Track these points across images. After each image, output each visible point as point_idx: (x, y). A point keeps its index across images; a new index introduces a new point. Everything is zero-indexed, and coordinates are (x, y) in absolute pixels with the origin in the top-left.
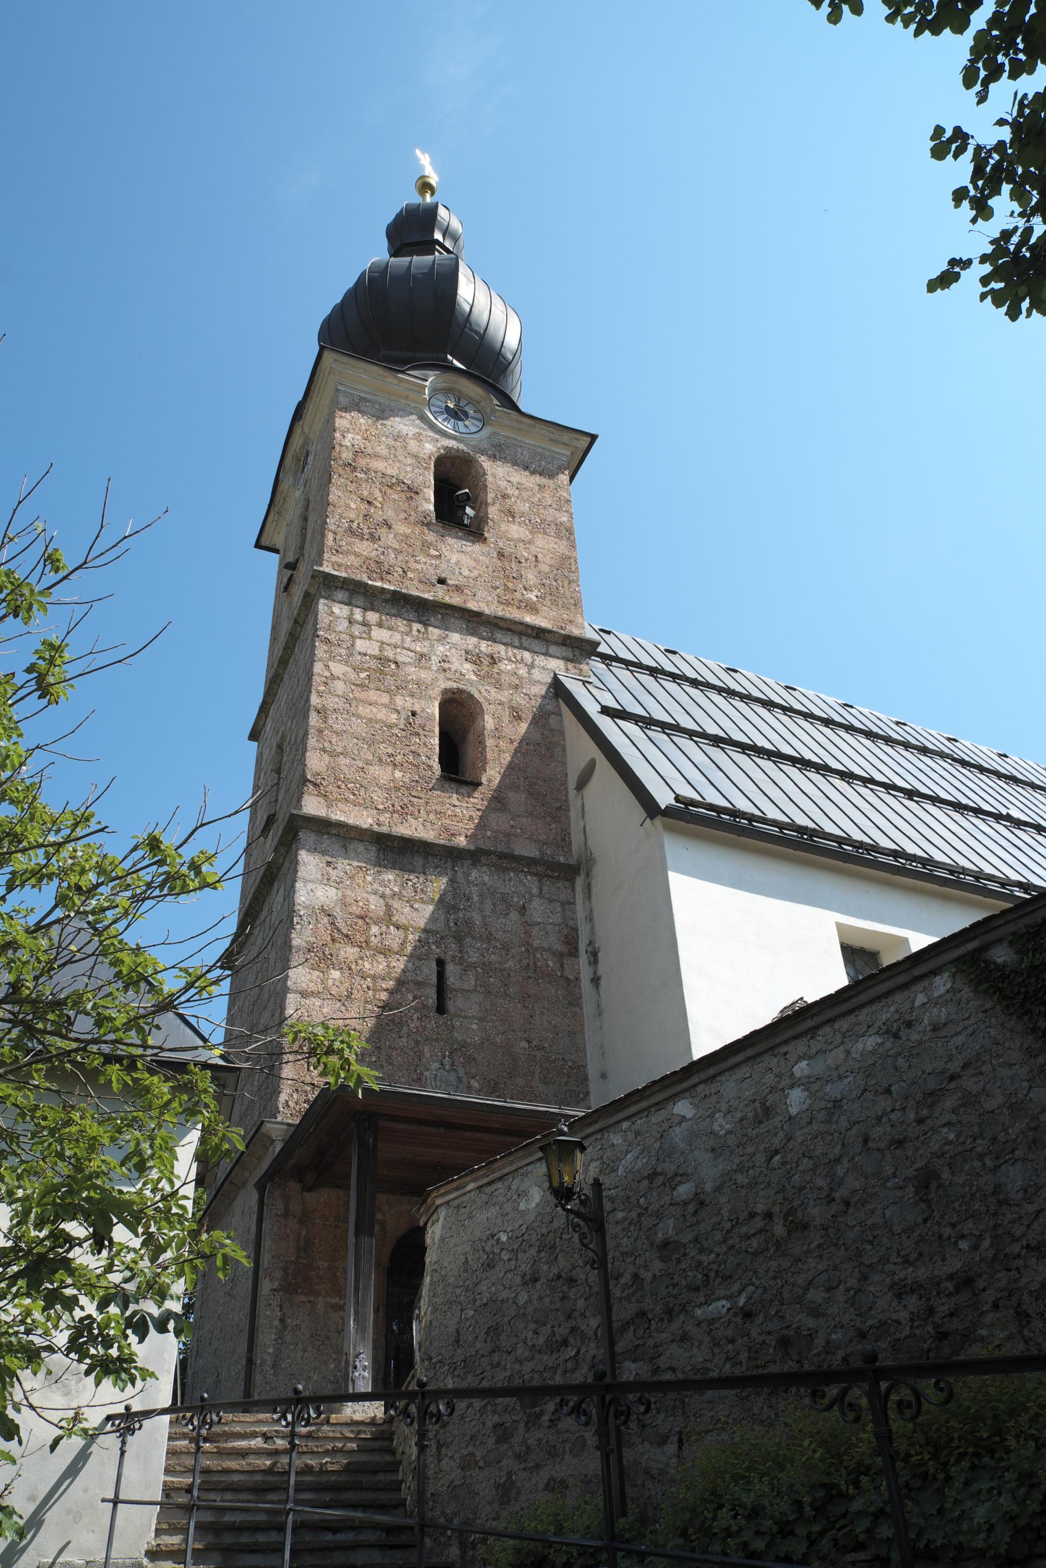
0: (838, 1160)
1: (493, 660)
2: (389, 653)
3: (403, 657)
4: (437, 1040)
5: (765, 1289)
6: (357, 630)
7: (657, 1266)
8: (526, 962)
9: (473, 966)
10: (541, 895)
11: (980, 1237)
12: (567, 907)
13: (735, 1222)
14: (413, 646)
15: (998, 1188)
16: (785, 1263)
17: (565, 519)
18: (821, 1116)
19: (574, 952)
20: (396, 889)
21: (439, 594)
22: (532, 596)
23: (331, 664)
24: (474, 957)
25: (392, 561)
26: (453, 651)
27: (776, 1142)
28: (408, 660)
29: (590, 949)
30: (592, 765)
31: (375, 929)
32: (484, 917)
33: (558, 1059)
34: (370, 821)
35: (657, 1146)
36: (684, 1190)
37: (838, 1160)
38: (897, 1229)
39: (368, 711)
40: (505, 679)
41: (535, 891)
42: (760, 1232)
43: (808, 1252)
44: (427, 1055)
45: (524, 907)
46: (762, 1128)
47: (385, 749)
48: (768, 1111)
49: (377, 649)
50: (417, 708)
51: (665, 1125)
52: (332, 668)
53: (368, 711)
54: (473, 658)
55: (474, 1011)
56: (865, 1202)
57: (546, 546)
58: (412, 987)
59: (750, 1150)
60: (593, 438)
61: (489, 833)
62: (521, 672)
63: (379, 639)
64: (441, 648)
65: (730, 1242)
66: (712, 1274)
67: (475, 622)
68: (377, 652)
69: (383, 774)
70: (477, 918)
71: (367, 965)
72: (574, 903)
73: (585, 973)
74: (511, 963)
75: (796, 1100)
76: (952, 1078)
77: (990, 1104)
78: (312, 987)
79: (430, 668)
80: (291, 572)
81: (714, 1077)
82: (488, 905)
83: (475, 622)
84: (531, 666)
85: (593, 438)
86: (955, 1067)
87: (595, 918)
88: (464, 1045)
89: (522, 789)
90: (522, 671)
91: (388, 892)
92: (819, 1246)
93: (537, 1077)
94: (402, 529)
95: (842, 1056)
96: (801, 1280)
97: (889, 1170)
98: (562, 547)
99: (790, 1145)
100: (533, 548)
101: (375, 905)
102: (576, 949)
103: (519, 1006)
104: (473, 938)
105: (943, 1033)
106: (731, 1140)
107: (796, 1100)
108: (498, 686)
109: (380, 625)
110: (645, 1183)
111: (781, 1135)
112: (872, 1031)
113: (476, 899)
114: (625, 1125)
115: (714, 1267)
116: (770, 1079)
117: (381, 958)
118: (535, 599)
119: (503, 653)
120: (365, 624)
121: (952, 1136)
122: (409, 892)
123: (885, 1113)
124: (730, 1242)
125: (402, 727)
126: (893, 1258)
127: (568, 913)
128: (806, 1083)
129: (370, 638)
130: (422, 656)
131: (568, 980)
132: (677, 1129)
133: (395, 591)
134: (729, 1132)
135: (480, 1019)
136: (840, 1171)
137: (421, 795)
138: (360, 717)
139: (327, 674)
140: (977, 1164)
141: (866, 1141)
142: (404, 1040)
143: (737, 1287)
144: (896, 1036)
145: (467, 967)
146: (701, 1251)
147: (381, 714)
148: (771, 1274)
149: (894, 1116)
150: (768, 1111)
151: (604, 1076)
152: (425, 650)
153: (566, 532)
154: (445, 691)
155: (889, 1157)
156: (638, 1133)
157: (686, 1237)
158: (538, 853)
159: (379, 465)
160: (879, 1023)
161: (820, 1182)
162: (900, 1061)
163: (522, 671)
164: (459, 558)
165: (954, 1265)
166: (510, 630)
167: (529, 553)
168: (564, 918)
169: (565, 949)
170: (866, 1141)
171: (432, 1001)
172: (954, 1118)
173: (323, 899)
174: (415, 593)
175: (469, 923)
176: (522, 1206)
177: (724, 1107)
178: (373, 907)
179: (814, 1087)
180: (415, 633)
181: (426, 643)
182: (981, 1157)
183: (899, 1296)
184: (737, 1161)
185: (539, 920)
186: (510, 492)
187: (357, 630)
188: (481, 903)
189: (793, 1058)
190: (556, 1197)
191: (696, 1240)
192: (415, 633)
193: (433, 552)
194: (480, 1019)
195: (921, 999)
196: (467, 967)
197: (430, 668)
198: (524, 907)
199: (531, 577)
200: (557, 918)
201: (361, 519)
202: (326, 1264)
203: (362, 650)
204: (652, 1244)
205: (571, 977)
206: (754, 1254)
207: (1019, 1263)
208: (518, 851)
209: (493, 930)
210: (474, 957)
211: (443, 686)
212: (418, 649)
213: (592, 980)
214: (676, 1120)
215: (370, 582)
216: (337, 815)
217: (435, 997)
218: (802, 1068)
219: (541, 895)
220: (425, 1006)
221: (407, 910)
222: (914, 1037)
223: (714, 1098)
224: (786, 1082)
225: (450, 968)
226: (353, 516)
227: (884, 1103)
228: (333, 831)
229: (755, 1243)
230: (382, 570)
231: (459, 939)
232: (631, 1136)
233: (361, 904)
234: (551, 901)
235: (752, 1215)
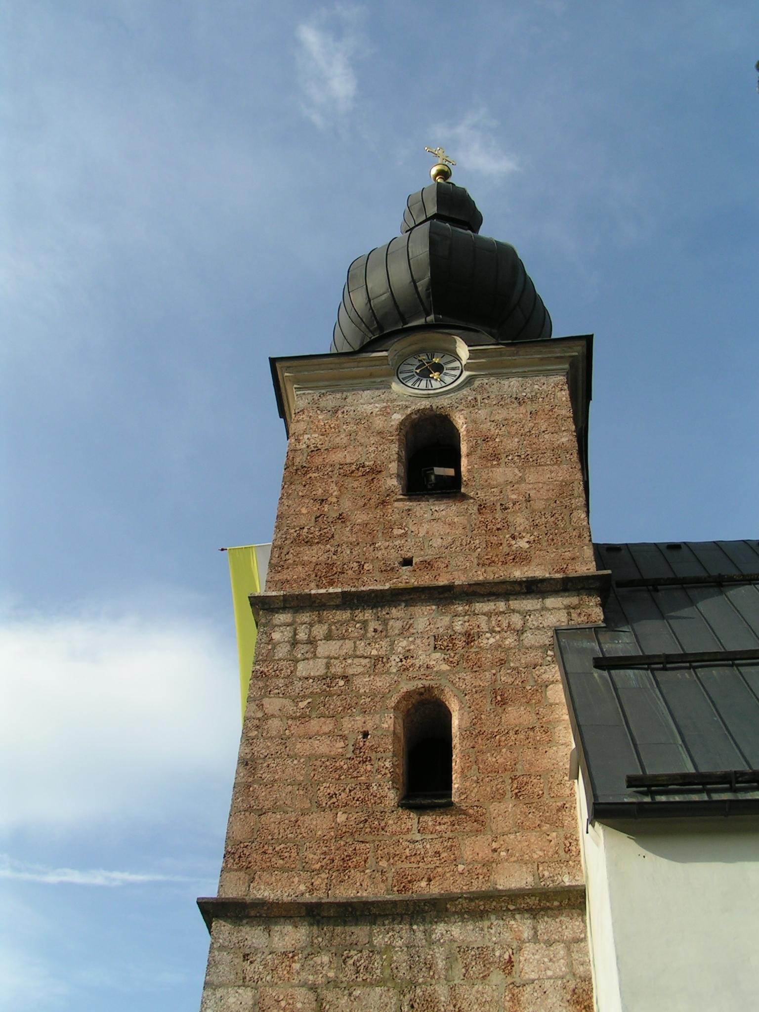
22: (523, 544)
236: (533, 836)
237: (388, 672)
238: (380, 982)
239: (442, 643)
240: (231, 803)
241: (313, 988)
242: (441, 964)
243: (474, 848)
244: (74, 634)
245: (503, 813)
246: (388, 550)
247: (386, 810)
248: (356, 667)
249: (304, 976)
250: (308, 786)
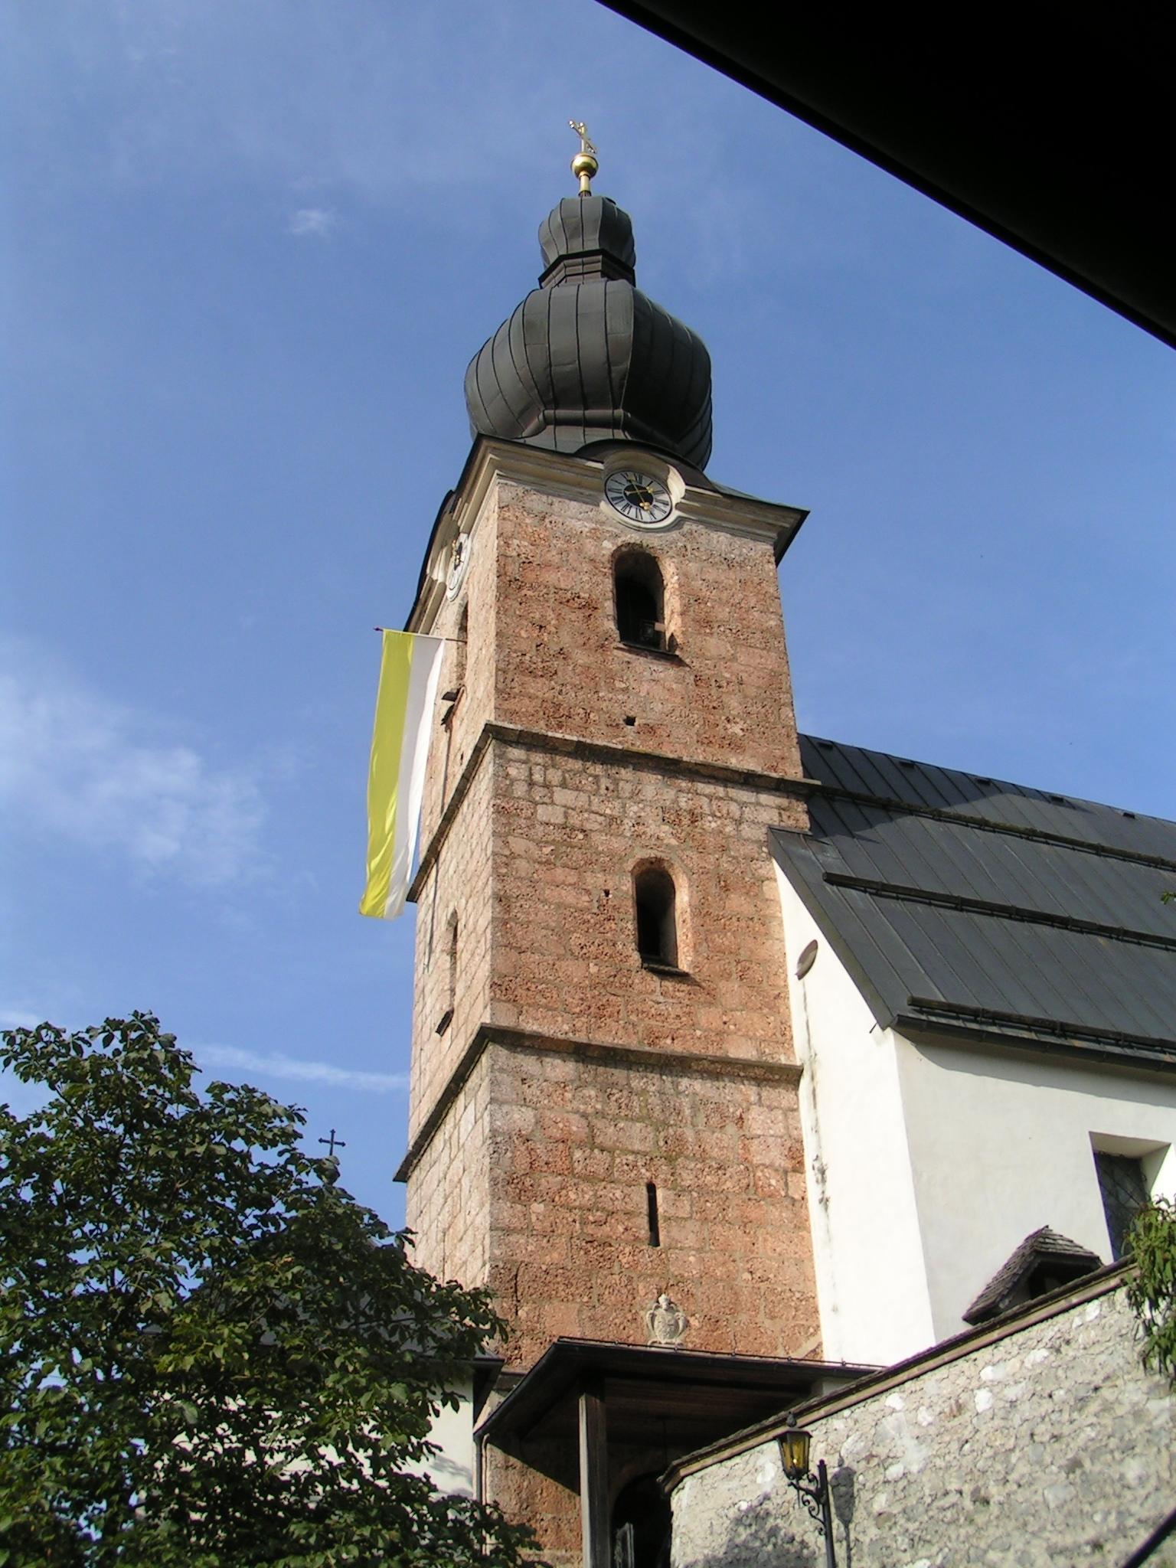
0: (1012, 1450)
1: (694, 817)
2: (575, 820)
3: (594, 823)
4: (651, 1276)
5: (956, 1552)
6: (538, 794)
7: (873, 1532)
8: (745, 1182)
9: (688, 1189)
10: (760, 1102)
11: (1109, 1513)
12: (790, 1114)
13: (935, 1498)
14: (602, 809)
15: (1122, 1477)
16: (971, 1530)
17: (772, 623)
18: (1001, 1413)
19: (798, 1167)
20: (599, 1106)
21: (630, 740)
22: (736, 729)
23: (510, 839)
24: (688, 1179)
25: (572, 702)
26: (648, 809)
27: (967, 1434)
28: (596, 827)
29: (817, 1164)
30: (813, 946)
31: (578, 1154)
32: (697, 1132)
33: (783, 1291)
34: (566, 1027)
35: (873, 1431)
36: (895, 1471)
37: (1012, 1450)
38: (1052, 1505)
39: (555, 894)
40: (711, 841)
41: (753, 1098)
42: (953, 1505)
43: (989, 1521)
44: (642, 1292)
45: (741, 1118)
46: (955, 1422)
47: (576, 939)
48: (960, 1408)
49: (561, 816)
50: (610, 886)
51: (879, 1415)
52: (512, 845)
53: (555, 894)
54: (671, 816)
55: (691, 1241)
56: (1031, 1484)
57: (752, 663)
58: (621, 1216)
59: (947, 1438)
60: (804, 514)
61: (698, 1033)
62: (728, 829)
63: (564, 802)
64: (635, 808)
65: (931, 1513)
66: (916, 1539)
67: (671, 768)
68: (561, 820)
69: (574, 970)
70: (689, 1135)
71: (572, 1196)
72: (796, 1110)
73: (813, 1193)
74: (729, 1184)
75: (983, 1400)
76: (1096, 1389)
77: (1120, 1411)
78: (516, 1223)
79: (622, 835)
80: (450, 703)
81: (918, 1376)
82: (701, 1119)
83: (671, 768)
84: (739, 822)
85: (804, 514)
86: (1097, 1380)
87: (822, 1129)
88: (680, 1280)
89: (734, 976)
90: (729, 829)
91: (590, 1110)
92: (997, 1518)
93: (762, 1313)
94: (581, 657)
95: (1018, 1365)
96: (983, 1545)
97: (1048, 1459)
98: (771, 661)
99: (977, 1437)
100: (735, 666)
101: (577, 1126)
102: (801, 1163)
103: (740, 1233)
104: (686, 1157)
105: (1092, 1351)
106: (933, 1430)
107: (983, 1400)
108: (701, 849)
109: (564, 785)
110: (863, 1464)
111: (970, 1428)
112: (1041, 1345)
113: (687, 1112)
114: (847, 1413)
115: (918, 1533)
116: (962, 1381)
117: (584, 1186)
118: (741, 733)
119: (706, 808)
120: (547, 785)
121: (1093, 1435)
122: (612, 1108)
123: (1047, 1414)
124: (931, 1513)
125: (595, 910)
126: (1049, 1527)
127: (790, 1121)
128: (992, 1386)
129: (553, 803)
130: (613, 818)
131: (794, 1200)
132: (889, 1418)
133: (579, 742)
134: (930, 1424)
135: (697, 1250)
136: (1014, 1458)
137: (620, 992)
138: (545, 902)
139: (507, 853)
140: (1109, 1457)
141: (1032, 1435)
142: (617, 1277)
143: (935, 1549)
144: (1058, 1351)
145: (680, 1192)
146: (908, 1520)
147: (569, 897)
148: (962, 1538)
149: (1054, 1417)
150: (960, 1408)
151: (835, 1310)
152: (616, 813)
153: (773, 640)
154: (642, 862)
155: (1048, 1449)
156: (856, 1421)
157: (896, 1509)
158: (754, 1053)
159: (550, 577)
160: (1046, 1340)
161: (999, 1467)
162: (1060, 1373)
163: (729, 829)
164: (649, 684)
165: (1090, 1533)
166: (714, 777)
167: (732, 674)
168: (787, 1128)
169: (788, 1164)
170: (1032, 1435)
171: (644, 1233)
172: (1094, 1420)
173: (520, 1123)
174: (600, 742)
175: (680, 1139)
176: (759, 1480)
177: (927, 1402)
178: (574, 1129)
179: (996, 1390)
180: (603, 791)
181: (617, 804)
182: (1112, 1452)
183: (1052, 1557)
184: (937, 1447)
185: (759, 1132)
186: (705, 593)
187: (538, 794)
188: (694, 1116)
189: (980, 1363)
190: (788, 1476)
191: (904, 1511)
192: (603, 791)
193: (619, 685)
194: (697, 1250)
195: (1077, 1321)
196: (680, 1192)
197: (622, 835)
198: (741, 1118)
199: (734, 704)
200: (779, 1129)
201: (534, 652)
202: (550, 1516)
203: (545, 819)
204: (869, 1514)
205: (797, 1197)
206: (949, 1523)
207: (1133, 1533)
208: (733, 1053)
209: (708, 1147)
210: (688, 1179)
211: (639, 856)
212: (608, 811)
213: (821, 1201)
214: (888, 1411)
215: (550, 734)
216: (530, 1026)
217: (647, 1227)
218: (988, 1374)
219: (760, 1102)
220: (637, 1239)
221: (611, 1130)
222: (1071, 1353)
223: (920, 1394)
224: (975, 1383)
225: (660, 1194)
226: (524, 647)
227: (1047, 1406)
228: (527, 1043)
229: (949, 1514)
230: (557, 714)
231: (670, 1160)
232: (851, 1423)
233: (561, 1125)
234: (771, 1109)
235: (946, 1493)
243: (708, 1017)
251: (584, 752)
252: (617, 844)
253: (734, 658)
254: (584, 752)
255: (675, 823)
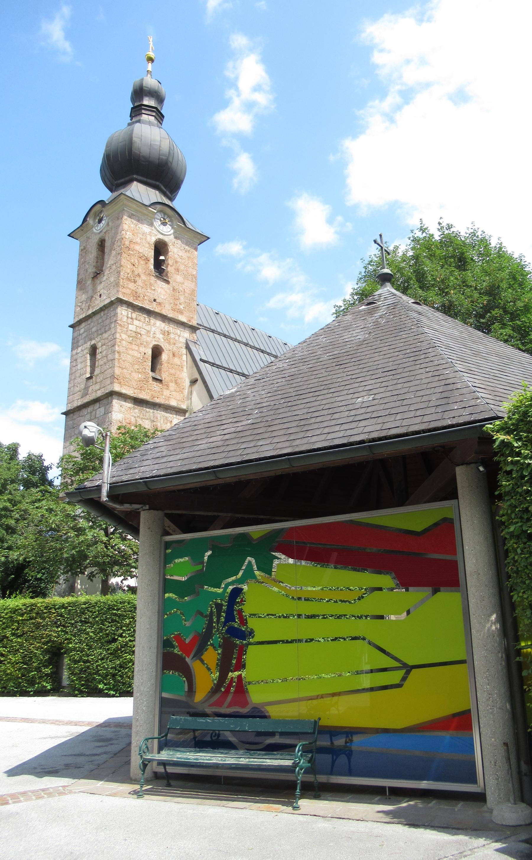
22: (181, 307)
67: (164, 318)
83: (164, 318)
84: (179, 336)
147: (136, 354)
181: (149, 326)
199: (182, 299)
236: (178, 394)
237: (149, 336)
238: (147, 419)
239: (164, 333)
240: (66, 385)
241: (135, 417)
242: (159, 418)
243: (166, 393)
244: (215, 775)
245: (172, 385)
246: (151, 295)
247: (173, 379)
248: (143, 332)
249: (133, 414)
250: (133, 365)
251: (142, 310)
252: (148, 339)
253: (183, 283)
254: (142, 310)
255: (164, 334)
